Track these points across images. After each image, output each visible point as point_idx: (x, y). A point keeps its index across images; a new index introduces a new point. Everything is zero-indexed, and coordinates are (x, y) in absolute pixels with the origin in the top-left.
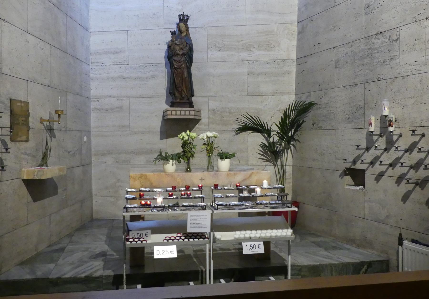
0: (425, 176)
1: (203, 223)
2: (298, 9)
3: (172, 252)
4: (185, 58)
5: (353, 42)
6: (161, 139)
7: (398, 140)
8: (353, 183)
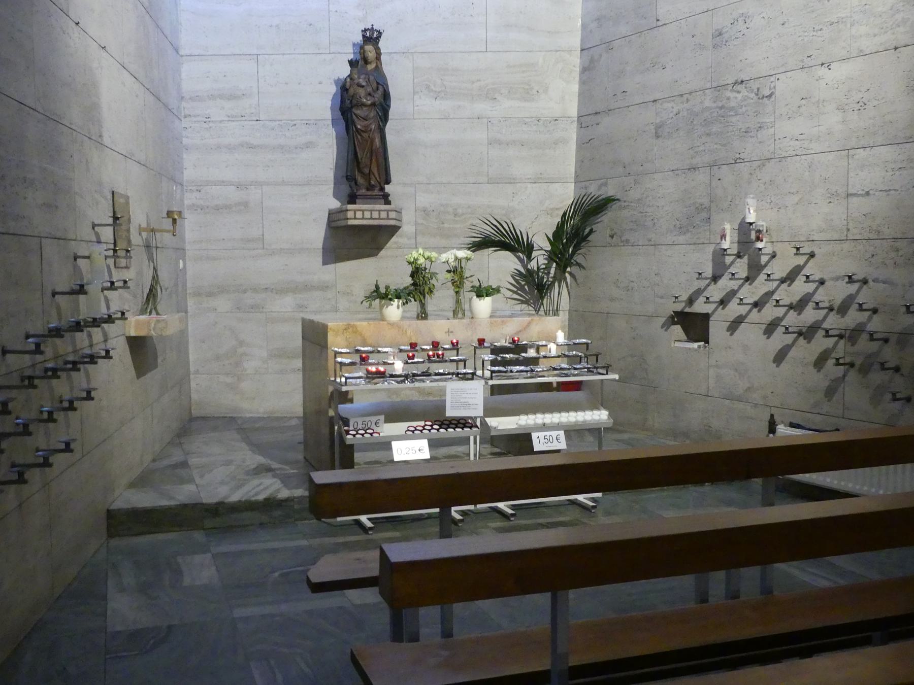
0: (813, 320)
1: (471, 401)
2: (583, 25)
3: (422, 450)
4: (375, 112)
5: (690, 93)
6: (325, 263)
7: (770, 263)
8: (684, 337)
